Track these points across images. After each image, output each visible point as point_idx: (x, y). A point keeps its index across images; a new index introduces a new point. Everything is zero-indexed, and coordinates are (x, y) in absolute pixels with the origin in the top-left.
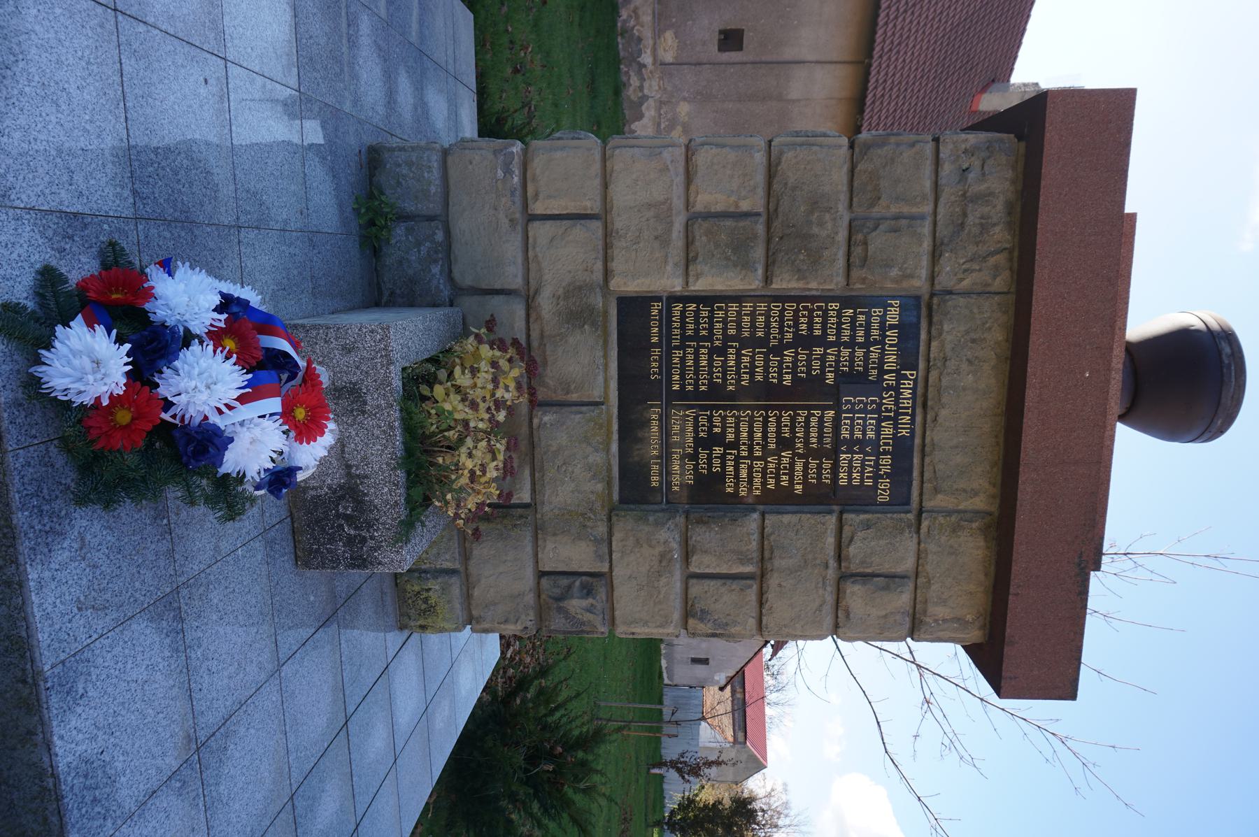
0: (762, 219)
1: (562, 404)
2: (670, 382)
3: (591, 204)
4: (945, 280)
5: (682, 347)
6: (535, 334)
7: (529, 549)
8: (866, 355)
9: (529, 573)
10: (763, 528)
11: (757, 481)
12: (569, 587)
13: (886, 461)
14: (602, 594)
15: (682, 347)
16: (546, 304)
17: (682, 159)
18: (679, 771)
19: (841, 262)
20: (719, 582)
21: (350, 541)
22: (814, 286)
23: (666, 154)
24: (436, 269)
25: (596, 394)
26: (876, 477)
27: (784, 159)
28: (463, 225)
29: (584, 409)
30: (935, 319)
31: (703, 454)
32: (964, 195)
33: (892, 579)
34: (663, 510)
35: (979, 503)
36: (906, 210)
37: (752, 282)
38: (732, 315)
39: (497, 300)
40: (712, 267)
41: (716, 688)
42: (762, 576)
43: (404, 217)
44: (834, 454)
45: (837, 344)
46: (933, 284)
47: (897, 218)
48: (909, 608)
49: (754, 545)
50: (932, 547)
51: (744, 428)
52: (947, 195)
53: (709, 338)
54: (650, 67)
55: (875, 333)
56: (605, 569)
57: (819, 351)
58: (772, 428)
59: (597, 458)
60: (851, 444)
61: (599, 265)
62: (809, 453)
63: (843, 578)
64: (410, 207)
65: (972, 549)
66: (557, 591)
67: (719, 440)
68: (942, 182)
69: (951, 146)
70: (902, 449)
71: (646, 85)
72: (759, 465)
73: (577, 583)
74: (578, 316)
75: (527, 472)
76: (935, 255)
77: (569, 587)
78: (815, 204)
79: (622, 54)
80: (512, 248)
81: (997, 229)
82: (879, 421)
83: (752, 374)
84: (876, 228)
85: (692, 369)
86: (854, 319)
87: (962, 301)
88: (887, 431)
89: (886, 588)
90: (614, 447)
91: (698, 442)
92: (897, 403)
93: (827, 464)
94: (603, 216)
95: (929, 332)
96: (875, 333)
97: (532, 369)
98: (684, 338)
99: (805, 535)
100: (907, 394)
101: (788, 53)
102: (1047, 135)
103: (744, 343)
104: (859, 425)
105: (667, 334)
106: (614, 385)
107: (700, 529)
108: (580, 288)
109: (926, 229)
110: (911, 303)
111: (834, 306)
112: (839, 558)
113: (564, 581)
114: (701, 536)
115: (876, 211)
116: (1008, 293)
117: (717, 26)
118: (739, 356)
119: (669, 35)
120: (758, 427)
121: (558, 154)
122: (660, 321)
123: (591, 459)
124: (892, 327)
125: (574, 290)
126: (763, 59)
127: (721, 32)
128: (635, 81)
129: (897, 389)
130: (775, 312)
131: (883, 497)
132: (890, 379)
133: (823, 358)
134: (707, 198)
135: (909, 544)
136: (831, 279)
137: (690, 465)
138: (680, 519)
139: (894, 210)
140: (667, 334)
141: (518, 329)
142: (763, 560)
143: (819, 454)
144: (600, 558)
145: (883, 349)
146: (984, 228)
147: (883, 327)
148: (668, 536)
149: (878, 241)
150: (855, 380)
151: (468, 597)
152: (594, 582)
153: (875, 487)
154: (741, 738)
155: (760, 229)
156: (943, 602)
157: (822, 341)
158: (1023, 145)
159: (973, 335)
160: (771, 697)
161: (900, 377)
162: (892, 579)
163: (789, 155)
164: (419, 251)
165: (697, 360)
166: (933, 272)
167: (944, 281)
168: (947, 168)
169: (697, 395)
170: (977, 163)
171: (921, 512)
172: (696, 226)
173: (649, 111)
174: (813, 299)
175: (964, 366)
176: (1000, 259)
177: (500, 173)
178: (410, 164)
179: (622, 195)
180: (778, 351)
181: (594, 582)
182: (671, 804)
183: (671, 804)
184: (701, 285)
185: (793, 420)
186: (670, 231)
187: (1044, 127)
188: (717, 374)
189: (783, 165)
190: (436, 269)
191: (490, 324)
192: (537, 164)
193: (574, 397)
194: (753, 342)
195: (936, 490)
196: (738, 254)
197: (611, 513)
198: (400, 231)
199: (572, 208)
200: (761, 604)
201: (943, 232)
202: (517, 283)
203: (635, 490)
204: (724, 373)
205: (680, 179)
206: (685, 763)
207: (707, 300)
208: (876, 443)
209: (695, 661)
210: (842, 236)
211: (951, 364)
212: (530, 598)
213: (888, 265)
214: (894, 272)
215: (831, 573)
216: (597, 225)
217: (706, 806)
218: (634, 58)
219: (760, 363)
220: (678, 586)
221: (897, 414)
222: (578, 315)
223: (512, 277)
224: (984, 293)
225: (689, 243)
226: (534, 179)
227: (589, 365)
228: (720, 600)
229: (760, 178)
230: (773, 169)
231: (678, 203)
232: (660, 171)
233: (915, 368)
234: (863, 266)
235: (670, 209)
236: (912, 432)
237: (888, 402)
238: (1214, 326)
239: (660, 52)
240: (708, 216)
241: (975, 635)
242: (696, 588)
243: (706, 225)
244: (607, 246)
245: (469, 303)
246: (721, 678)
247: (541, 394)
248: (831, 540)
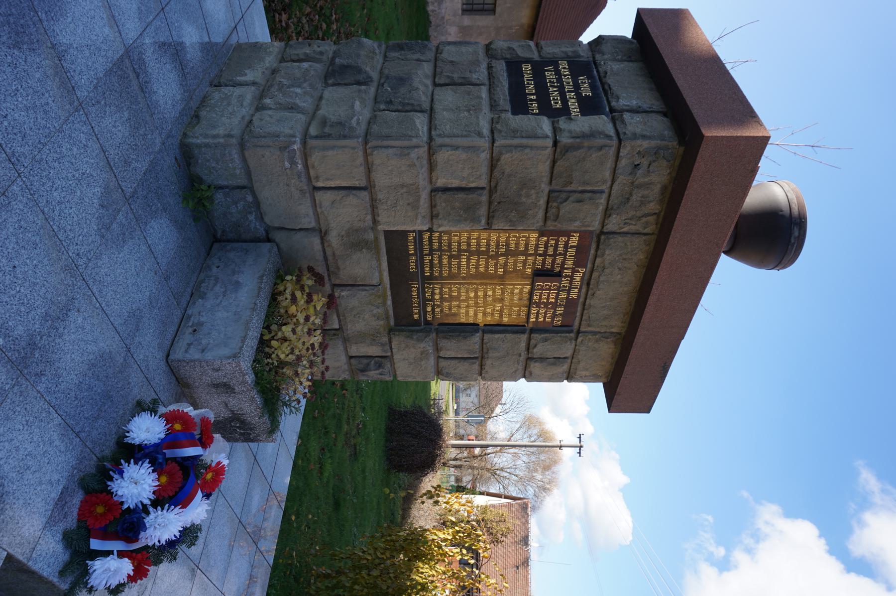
0: (486, 192)
2: (423, 271)
8: (553, 262)
9: (343, 358)
10: (483, 340)
12: (368, 364)
16: (334, 239)
17: (425, 156)
20: (456, 361)
23: (414, 154)
24: (252, 217)
27: (502, 158)
28: (266, 194)
29: (367, 288)
30: (601, 247)
32: (632, 183)
34: (421, 331)
40: (449, 221)
46: (603, 227)
52: (621, 179)
56: (389, 354)
61: (369, 217)
63: (529, 359)
66: (361, 366)
68: (619, 171)
69: (629, 148)
73: (373, 362)
75: (335, 317)
77: (368, 364)
81: (652, 204)
84: (566, 200)
86: (547, 243)
88: (563, 295)
89: (554, 364)
90: (389, 302)
92: (571, 283)
94: (368, 187)
95: (596, 251)
98: (431, 252)
100: (578, 279)
102: (697, 164)
106: (386, 275)
108: (357, 230)
109: (603, 200)
113: (365, 361)
114: (443, 343)
116: (653, 234)
118: (468, 260)
121: (330, 153)
122: (415, 242)
123: (375, 312)
124: (572, 247)
129: (572, 277)
132: (568, 272)
138: (434, 335)
145: (565, 258)
147: (566, 246)
152: (380, 361)
155: (484, 198)
158: (682, 149)
159: (624, 257)
161: (574, 271)
164: (237, 207)
165: (440, 261)
166: (604, 222)
167: (611, 226)
168: (623, 162)
170: (645, 162)
171: (579, 332)
172: (438, 196)
175: (616, 271)
176: (651, 219)
177: (287, 165)
179: (381, 179)
180: (496, 256)
186: (418, 201)
187: (695, 160)
189: (502, 161)
190: (252, 217)
197: (391, 331)
201: (614, 201)
204: (459, 268)
210: (542, 202)
211: (607, 271)
212: (346, 367)
216: (365, 194)
221: (570, 288)
225: (432, 206)
226: (313, 167)
230: (494, 162)
231: (422, 181)
232: (409, 166)
233: (586, 268)
234: (555, 220)
235: (417, 188)
236: (579, 297)
240: (445, 190)
241: (605, 380)
243: (444, 196)
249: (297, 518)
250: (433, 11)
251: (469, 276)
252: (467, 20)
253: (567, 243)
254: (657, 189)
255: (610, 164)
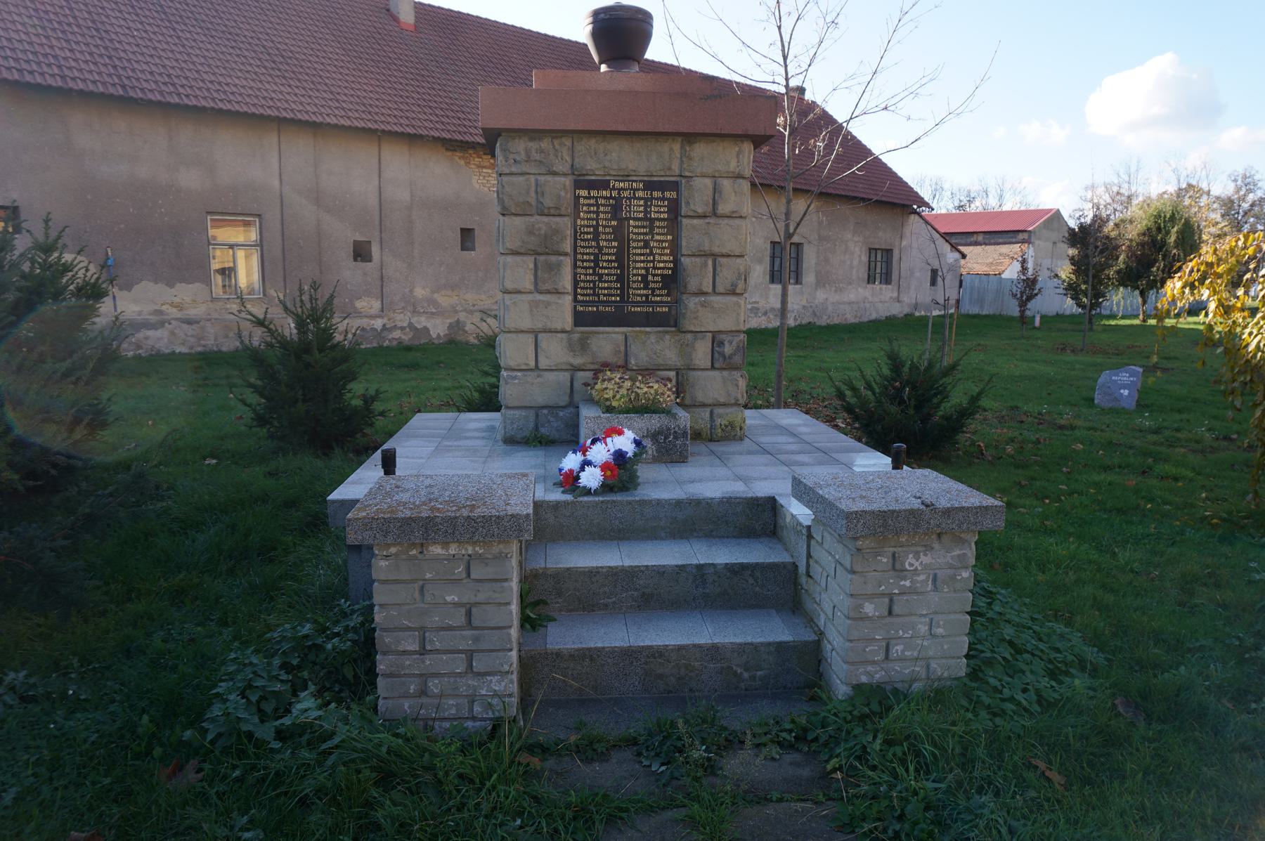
1: (626, 355)
3: (531, 338)
4: (565, 168)
5: (598, 295)
6: (592, 367)
7: (699, 373)
11: (666, 258)
13: (655, 194)
14: (723, 337)
15: (598, 295)
16: (578, 361)
18: (1030, 298)
19: (558, 219)
21: (676, 438)
22: (569, 232)
23: (508, 303)
25: (621, 338)
26: (663, 199)
28: (540, 400)
31: (652, 285)
33: (716, 189)
35: (677, 147)
36: (533, 189)
37: (568, 262)
38: (583, 271)
39: (576, 385)
41: (963, 262)
42: (714, 256)
43: (536, 428)
44: (652, 220)
45: (597, 220)
47: (537, 192)
48: (731, 181)
49: (698, 260)
50: (699, 171)
51: (639, 265)
53: (594, 282)
54: (385, 320)
55: (592, 201)
57: (601, 229)
58: (639, 251)
59: (653, 338)
60: (646, 212)
62: (651, 233)
63: (715, 214)
64: (532, 425)
65: (700, 149)
67: (644, 277)
70: (649, 186)
71: (399, 324)
72: (657, 257)
74: (583, 345)
76: (555, 174)
78: (530, 232)
79: (375, 345)
80: (551, 377)
82: (635, 198)
83: (611, 261)
85: (608, 289)
87: (576, 160)
88: (640, 194)
89: (720, 193)
90: (648, 329)
91: (646, 288)
93: (657, 224)
94: (535, 333)
96: (592, 201)
97: (606, 365)
98: (594, 294)
99: (693, 233)
100: (622, 185)
101: (373, 201)
103: (597, 265)
104: (637, 208)
105: (592, 303)
106: (617, 329)
107: (689, 287)
109: (542, 178)
110: (578, 184)
111: (579, 222)
112: (705, 217)
113: (716, 355)
114: (693, 285)
115: (534, 203)
117: (352, 264)
119: (359, 304)
120: (638, 258)
125: (571, 347)
126: (377, 223)
127: (355, 260)
128: (397, 334)
129: (620, 190)
130: (582, 250)
131: (674, 195)
132: (614, 194)
133: (604, 227)
134: (528, 284)
135: (698, 182)
136: (565, 224)
137: (658, 292)
138: (684, 297)
139: (533, 194)
140: (592, 303)
141: (590, 374)
142: (706, 255)
143: (652, 228)
144: (704, 338)
146: (542, 151)
148: (692, 303)
149: (548, 202)
150: (616, 209)
151: (724, 405)
152: (717, 340)
153: (668, 199)
154: (1025, 236)
155: (542, 258)
156: (728, 163)
157: (596, 227)
160: (993, 203)
161: (614, 188)
162: (716, 189)
163: (508, 245)
168: (514, 169)
169: (622, 289)
170: (511, 156)
173: (421, 322)
174: (576, 232)
175: (608, 157)
176: (556, 142)
178: (512, 423)
179: (526, 323)
180: (600, 248)
181: (717, 340)
182: (1069, 306)
183: (1069, 306)
184: (569, 287)
185: (634, 241)
188: (612, 278)
190: (561, 414)
191: (586, 385)
192: (512, 364)
193: (622, 348)
194: (596, 261)
195: (670, 169)
196: (554, 269)
198: (542, 430)
199: (532, 347)
200: (729, 256)
202: (567, 375)
203: (669, 321)
205: (519, 296)
206: (1022, 293)
207: (576, 283)
208: (646, 200)
209: (933, 282)
210: (545, 219)
211: (607, 164)
212: (725, 373)
213: (559, 197)
214: (563, 194)
215: (712, 221)
216: (540, 336)
217: (1075, 272)
218: (379, 334)
219: (606, 258)
220: (719, 298)
222: (582, 346)
223: (564, 377)
224: (573, 149)
225: (549, 292)
227: (607, 341)
228: (726, 277)
229: (518, 258)
231: (530, 297)
237: (626, 194)
238: (590, 20)
239: (373, 311)
240: (536, 283)
242: (720, 289)
244: (550, 331)
245: (577, 397)
246: (952, 256)
247: (621, 362)
248: (695, 221)
249: (1151, 500)
250: (795, 319)
251: (621, 267)
252: (809, 278)
253: (585, 198)
254: (530, 144)
255: (514, 179)
